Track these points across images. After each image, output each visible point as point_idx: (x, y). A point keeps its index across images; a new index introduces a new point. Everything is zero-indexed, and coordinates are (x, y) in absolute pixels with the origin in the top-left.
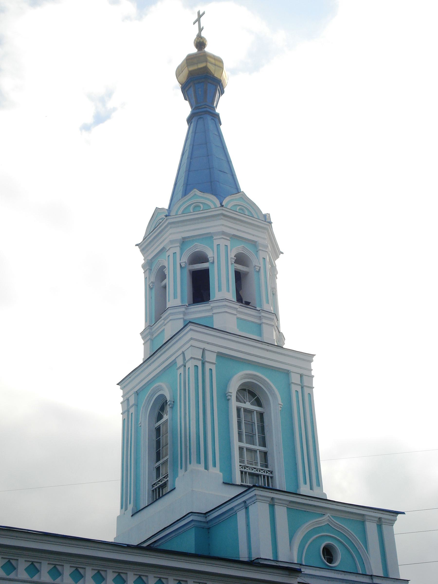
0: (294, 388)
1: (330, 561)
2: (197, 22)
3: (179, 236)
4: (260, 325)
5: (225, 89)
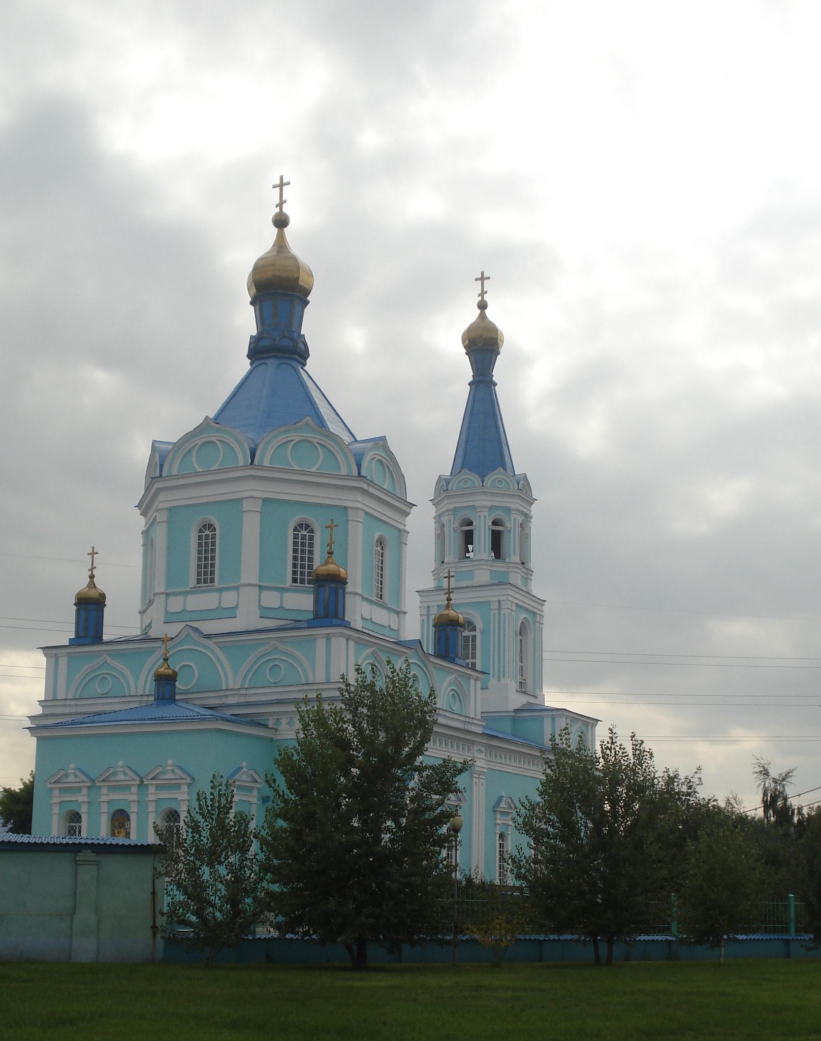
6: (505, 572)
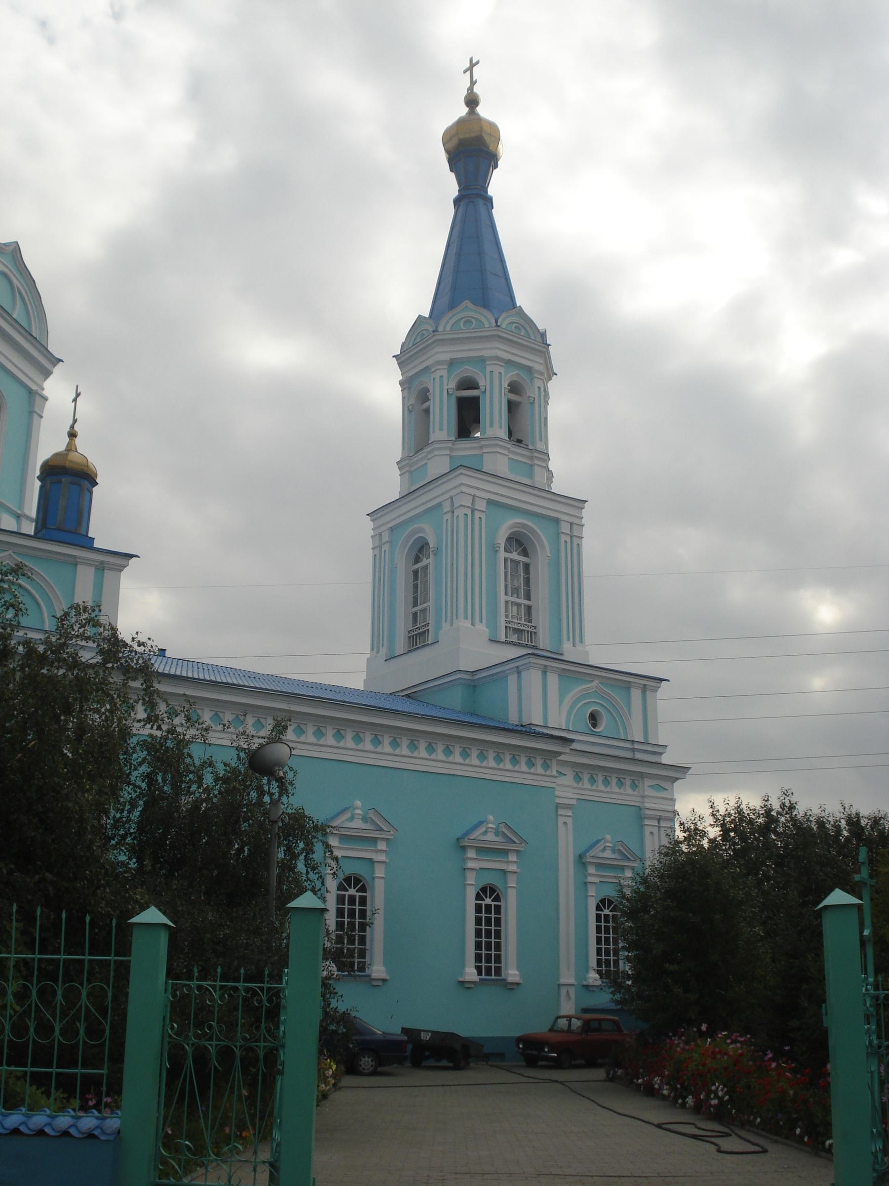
0: (563, 538)
1: (594, 726)
2: (469, 72)
3: (447, 357)
4: (531, 466)
5: (499, 163)
6: (475, 455)
